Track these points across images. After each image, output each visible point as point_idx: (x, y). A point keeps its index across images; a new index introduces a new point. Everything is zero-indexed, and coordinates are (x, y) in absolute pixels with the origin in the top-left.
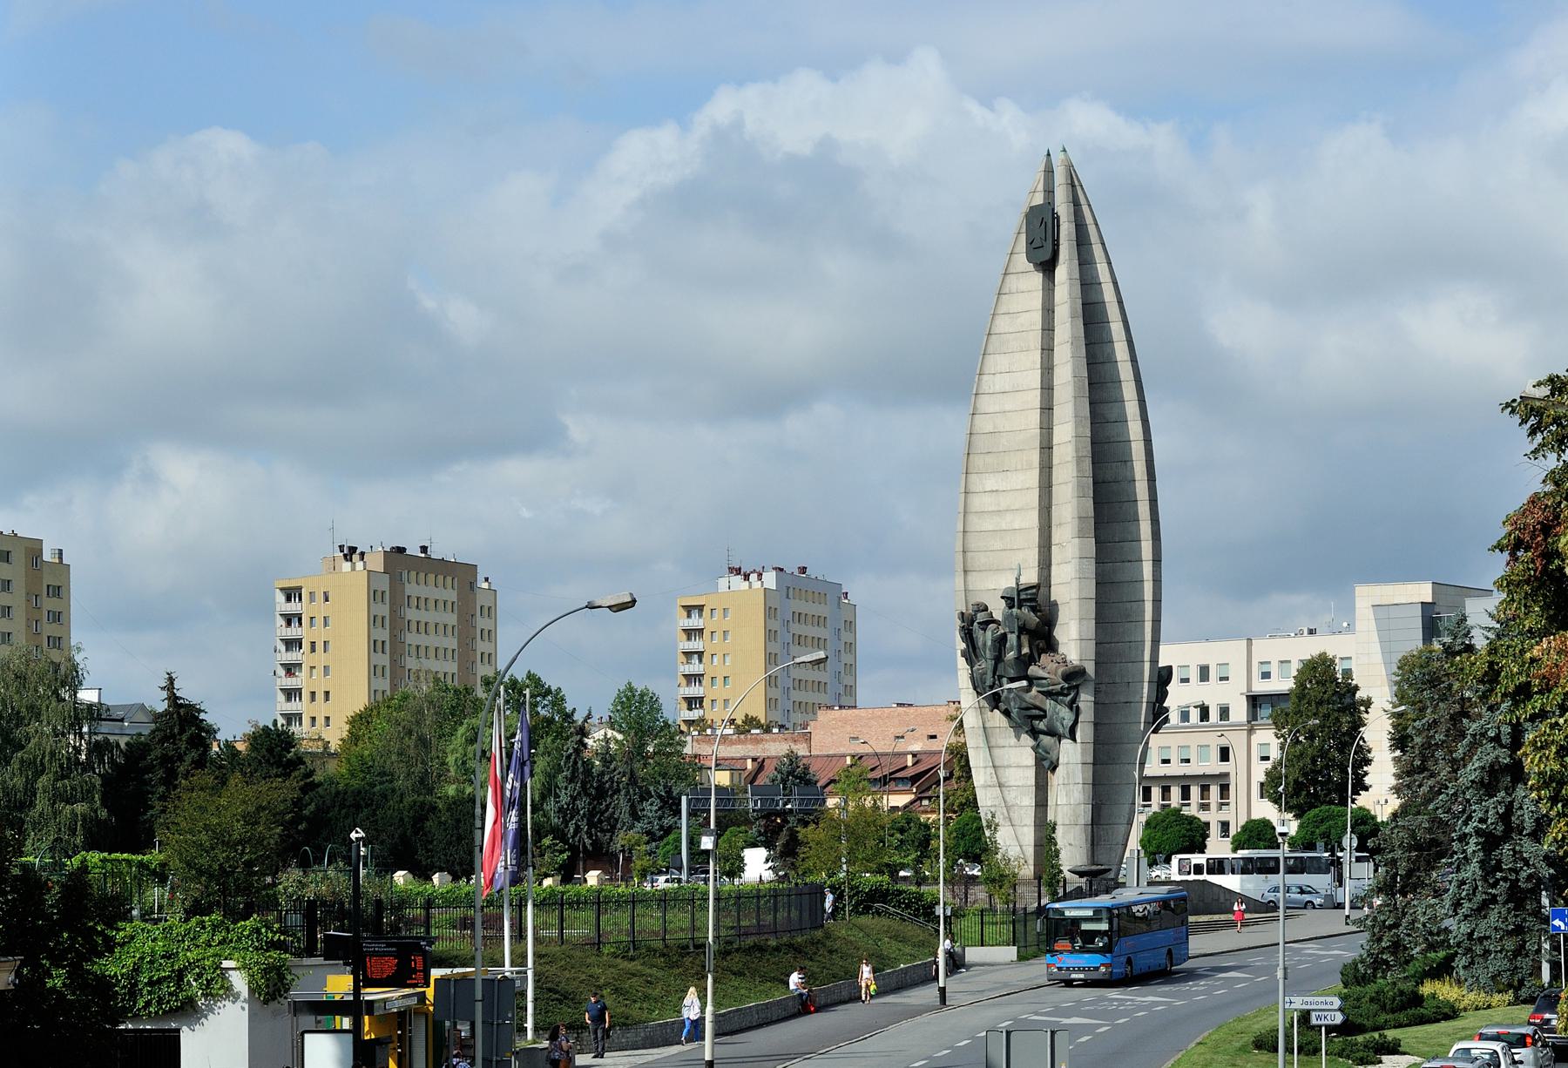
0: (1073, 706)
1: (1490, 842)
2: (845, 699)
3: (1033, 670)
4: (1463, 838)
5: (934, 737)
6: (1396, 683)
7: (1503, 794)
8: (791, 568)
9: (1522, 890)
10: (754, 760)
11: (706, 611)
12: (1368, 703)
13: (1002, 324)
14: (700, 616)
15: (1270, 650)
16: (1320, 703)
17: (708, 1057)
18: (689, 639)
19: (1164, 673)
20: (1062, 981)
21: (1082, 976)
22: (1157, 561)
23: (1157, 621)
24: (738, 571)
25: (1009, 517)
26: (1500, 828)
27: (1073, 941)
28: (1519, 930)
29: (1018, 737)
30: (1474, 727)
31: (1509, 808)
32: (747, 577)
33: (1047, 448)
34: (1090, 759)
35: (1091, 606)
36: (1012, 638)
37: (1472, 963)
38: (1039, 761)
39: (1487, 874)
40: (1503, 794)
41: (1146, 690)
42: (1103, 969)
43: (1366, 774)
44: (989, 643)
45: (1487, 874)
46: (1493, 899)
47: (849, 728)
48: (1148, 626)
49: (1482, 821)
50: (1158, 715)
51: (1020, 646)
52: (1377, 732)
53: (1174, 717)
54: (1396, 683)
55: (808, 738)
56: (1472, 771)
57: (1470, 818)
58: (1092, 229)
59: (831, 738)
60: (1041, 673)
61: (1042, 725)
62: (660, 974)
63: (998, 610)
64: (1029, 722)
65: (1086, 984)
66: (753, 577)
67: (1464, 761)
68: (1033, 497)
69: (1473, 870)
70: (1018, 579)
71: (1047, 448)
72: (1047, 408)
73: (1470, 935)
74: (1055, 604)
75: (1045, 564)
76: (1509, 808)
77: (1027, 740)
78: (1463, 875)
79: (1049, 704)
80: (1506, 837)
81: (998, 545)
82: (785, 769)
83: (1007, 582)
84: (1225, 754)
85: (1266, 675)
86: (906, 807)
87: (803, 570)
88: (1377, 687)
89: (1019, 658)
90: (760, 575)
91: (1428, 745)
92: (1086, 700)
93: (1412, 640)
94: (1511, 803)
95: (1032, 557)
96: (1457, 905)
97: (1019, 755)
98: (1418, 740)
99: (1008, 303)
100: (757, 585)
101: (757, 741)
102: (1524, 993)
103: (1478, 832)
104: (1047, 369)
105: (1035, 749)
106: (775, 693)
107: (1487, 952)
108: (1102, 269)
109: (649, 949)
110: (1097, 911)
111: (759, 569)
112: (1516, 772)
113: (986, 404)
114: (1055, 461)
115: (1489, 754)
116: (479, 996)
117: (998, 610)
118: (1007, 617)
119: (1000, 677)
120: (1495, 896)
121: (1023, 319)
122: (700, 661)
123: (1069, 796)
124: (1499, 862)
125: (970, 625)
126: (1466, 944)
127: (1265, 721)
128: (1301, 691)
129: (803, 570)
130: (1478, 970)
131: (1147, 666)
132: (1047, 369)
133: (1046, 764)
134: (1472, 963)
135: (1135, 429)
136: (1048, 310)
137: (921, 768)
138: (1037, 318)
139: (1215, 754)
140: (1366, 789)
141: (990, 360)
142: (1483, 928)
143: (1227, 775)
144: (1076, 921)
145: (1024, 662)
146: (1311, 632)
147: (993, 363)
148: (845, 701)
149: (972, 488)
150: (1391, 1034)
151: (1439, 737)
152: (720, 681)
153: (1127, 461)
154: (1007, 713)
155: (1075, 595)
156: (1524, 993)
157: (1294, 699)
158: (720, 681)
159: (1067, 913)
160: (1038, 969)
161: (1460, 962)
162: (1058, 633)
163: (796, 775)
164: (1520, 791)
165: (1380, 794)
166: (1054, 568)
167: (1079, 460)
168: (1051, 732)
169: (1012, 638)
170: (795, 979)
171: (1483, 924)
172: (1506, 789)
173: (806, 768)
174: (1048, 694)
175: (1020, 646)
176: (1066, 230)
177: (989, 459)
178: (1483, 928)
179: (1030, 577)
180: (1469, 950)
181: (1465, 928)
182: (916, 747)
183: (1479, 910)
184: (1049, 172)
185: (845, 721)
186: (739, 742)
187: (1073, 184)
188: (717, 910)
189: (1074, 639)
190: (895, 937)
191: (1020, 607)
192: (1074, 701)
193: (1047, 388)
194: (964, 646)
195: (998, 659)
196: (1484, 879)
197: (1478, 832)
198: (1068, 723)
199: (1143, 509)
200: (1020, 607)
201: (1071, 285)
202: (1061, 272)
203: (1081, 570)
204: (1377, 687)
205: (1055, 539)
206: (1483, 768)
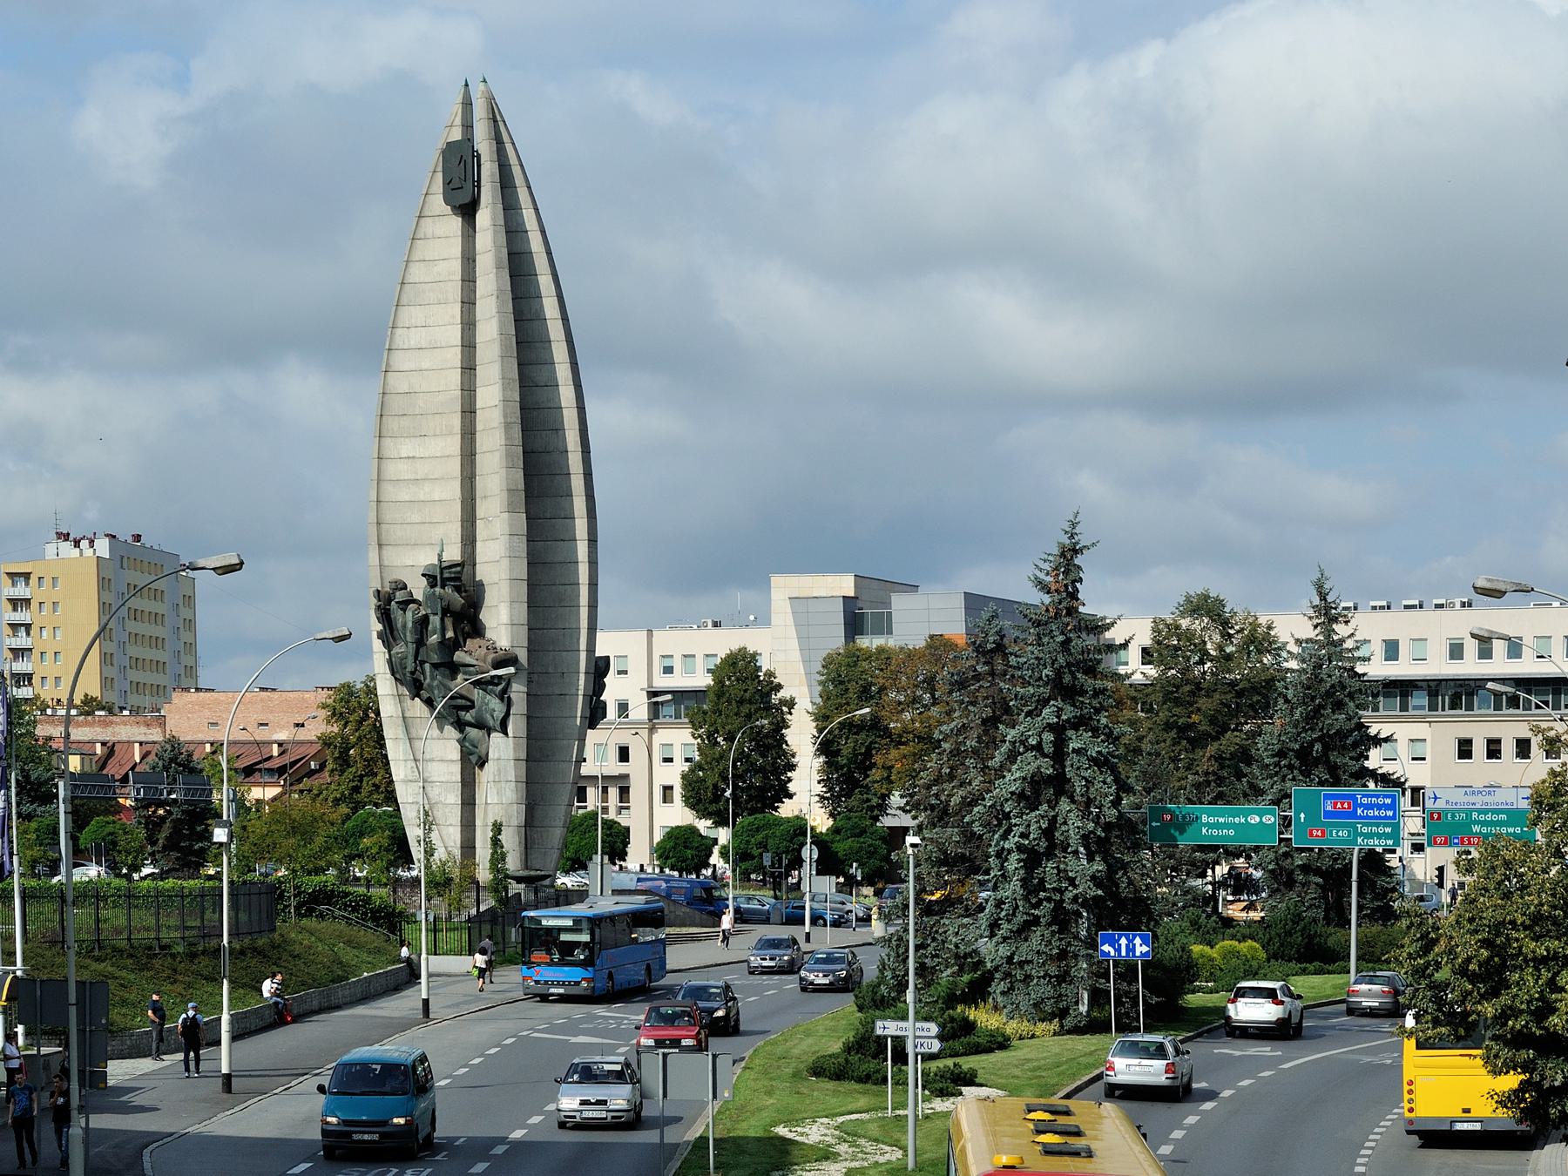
0: (504, 696)
1: (1032, 859)
2: (187, 679)
3: (459, 656)
4: (1002, 855)
5: (215, 724)
6: (820, 683)
7: (1045, 807)
8: (125, 535)
9: (1066, 912)
10: (103, 744)
11: (33, 580)
12: (791, 704)
13: (416, 273)
14: (27, 584)
15: (671, 642)
16: (741, 702)
17: (225, 1070)
18: (15, 609)
19: (602, 664)
20: (536, 995)
21: (561, 991)
22: (593, 541)
23: (593, 606)
24: (66, 537)
25: (427, 487)
26: (1043, 844)
27: (549, 952)
28: (1063, 955)
29: (441, 729)
30: (1012, 734)
31: (1053, 821)
32: (77, 543)
33: (469, 411)
34: (523, 756)
35: (523, 588)
36: (435, 621)
37: (1012, 988)
38: (465, 756)
39: (1029, 893)
40: (1045, 807)
41: (581, 687)
42: (584, 984)
43: (790, 780)
44: (410, 625)
45: (1029, 893)
46: (1036, 921)
47: (207, 713)
48: (584, 613)
49: (1023, 836)
50: (596, 713)
51: (443, 630)
52: (801, 736)
53: (612, 712)
54: (820, 683)
55: (162, 722)
56: (1013, 780)
57: (1008, 831)
58: (516, 170)
59: (190, 720)
60: (468, 660)
61: (468, 716)
62: (132, 977)
63: (418, 588)
64: (457, 714)
65: (563, 999)
66: (84, 544)
67: (1000, 772)
68: (455, 467)
69: (1013, 889)
70: (440, 556)
71: (469, 411)
72: (469, 368)
73: (1010, 959)
74: (481, 585)
75: (469, 540)
76: (1053, 821)
77: (451, 731)
78: (1001, 894)
79: (477, 694)
80: (1049, 854)
81: (416, 518)
82: (167, 756)
83: (428, 558)
84: (624, 754)
85: (668, 670)
86: (274, 799)
87: (138, 538)
88: (800, 689)
89: (443, 642)
90: (92, 542)
91: (956, 753)
92: (518, 691)
93: (834, 639)
94: (1055, 817)
95: (454, 532)
96: (994, 926)
97: (445, 748)
98: (946, 746)
99: (423, 250)
100: (88, 552)
101: (105, 724)
102: (1069, 1022)
103: (1020, 848)
104: (469, 325)
105: (461, 742)
106: (112, 672)
107: (1028, 977)
108: (528, 215)
109: (114, 949)
110: (577, 921)
111: (91, 536)
112: (1060, 784)
113: (400, 361)
114: (479, 427)
115: (1029, 764)
116: (72, 999)
117: (418, 588)
118: (429, 597)
119: (423, 663)
120: (1037, 918)
121: (441, 267)
122: (28, 634)
123: (500, 792)
124: (1042, 881)
125: (388, 604)
126: (1005, 967)
127: (667, 720)
128: (719, 690)
129: (138, 538)
130: (1019, 997)
131: (583, 656)
132: (469, 325)
133: (474, 759)
134: (1012, 988)
135: (566, 394)
136: (469, 259)
137: (287, 759)
138: (455, 267)
139: (613, 754)
140: (790, 796)
141: (403, 311)
142: (1024, 951)
143: (626, 777)
144: (550, 931)
145: (450, 647)
146: (716, 625)
147: (408, 315)
148: (185, 683)
149: (386, 453)
150: (968, 1063)
151: (971, 743)
152: (49, 656)
153: (559, 430)
154: (430, 703)
155: (505, 575)
156: (1069, 1022)
157: (711, 696)
158: (49, 656)
159: (544, 923)
160: (511, 977)
161: (997, 987)
162: (485, 616)
163: (177, 761)
164: (1064, 805)
165: (805, 798)
166: (479, 544)
167: (507, 426)
168: (480, 725)
169: (435, 621)
170: (268, 987)
171: (1024, 947)
172: (1049, 802)
173: (190, 755)
174: (477, 683)
175: (443, 630)
176: (489, 170)
177: (405, 422)
178: (1024, 951)
179: (453, 554)
180: (1008, 975)
181: (1004, 951)
182: (282, 736)
183: (1019, 932)
184: (467, 104)
185: (203, 705)
186: (87, 724)
187: (495, 119)
188: (234, 906)
189: (503, 621)
190: (349, 943)
191: (443, 587)
192: (505, 691)
193: (469, 346)
194: (380, 627)
195: (420, 643)
196: (1026, 898)
197: (1020, 848)
198: (499, 714)
199: (577, 483)
200: (443, 587)
201: (495, 232)
202: (484, 217)
203: (511, 548)
204: (800, 689)
205: (480, 513)
206: (1024, 779)
